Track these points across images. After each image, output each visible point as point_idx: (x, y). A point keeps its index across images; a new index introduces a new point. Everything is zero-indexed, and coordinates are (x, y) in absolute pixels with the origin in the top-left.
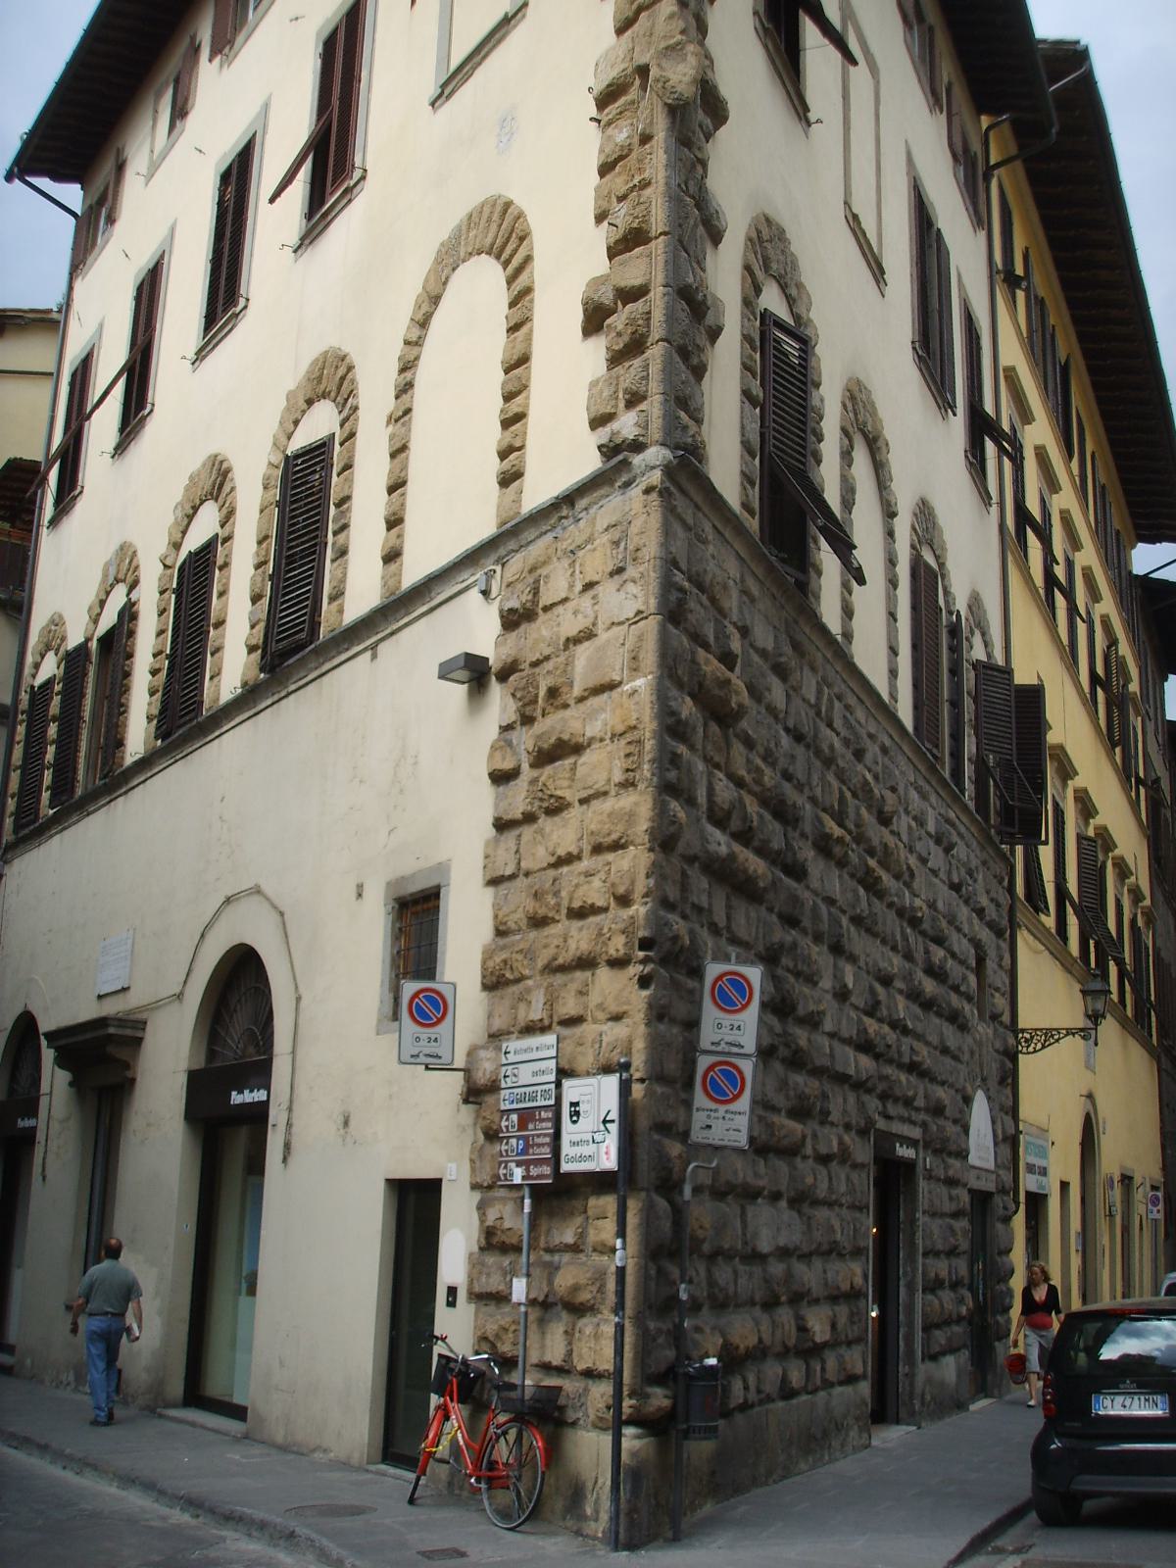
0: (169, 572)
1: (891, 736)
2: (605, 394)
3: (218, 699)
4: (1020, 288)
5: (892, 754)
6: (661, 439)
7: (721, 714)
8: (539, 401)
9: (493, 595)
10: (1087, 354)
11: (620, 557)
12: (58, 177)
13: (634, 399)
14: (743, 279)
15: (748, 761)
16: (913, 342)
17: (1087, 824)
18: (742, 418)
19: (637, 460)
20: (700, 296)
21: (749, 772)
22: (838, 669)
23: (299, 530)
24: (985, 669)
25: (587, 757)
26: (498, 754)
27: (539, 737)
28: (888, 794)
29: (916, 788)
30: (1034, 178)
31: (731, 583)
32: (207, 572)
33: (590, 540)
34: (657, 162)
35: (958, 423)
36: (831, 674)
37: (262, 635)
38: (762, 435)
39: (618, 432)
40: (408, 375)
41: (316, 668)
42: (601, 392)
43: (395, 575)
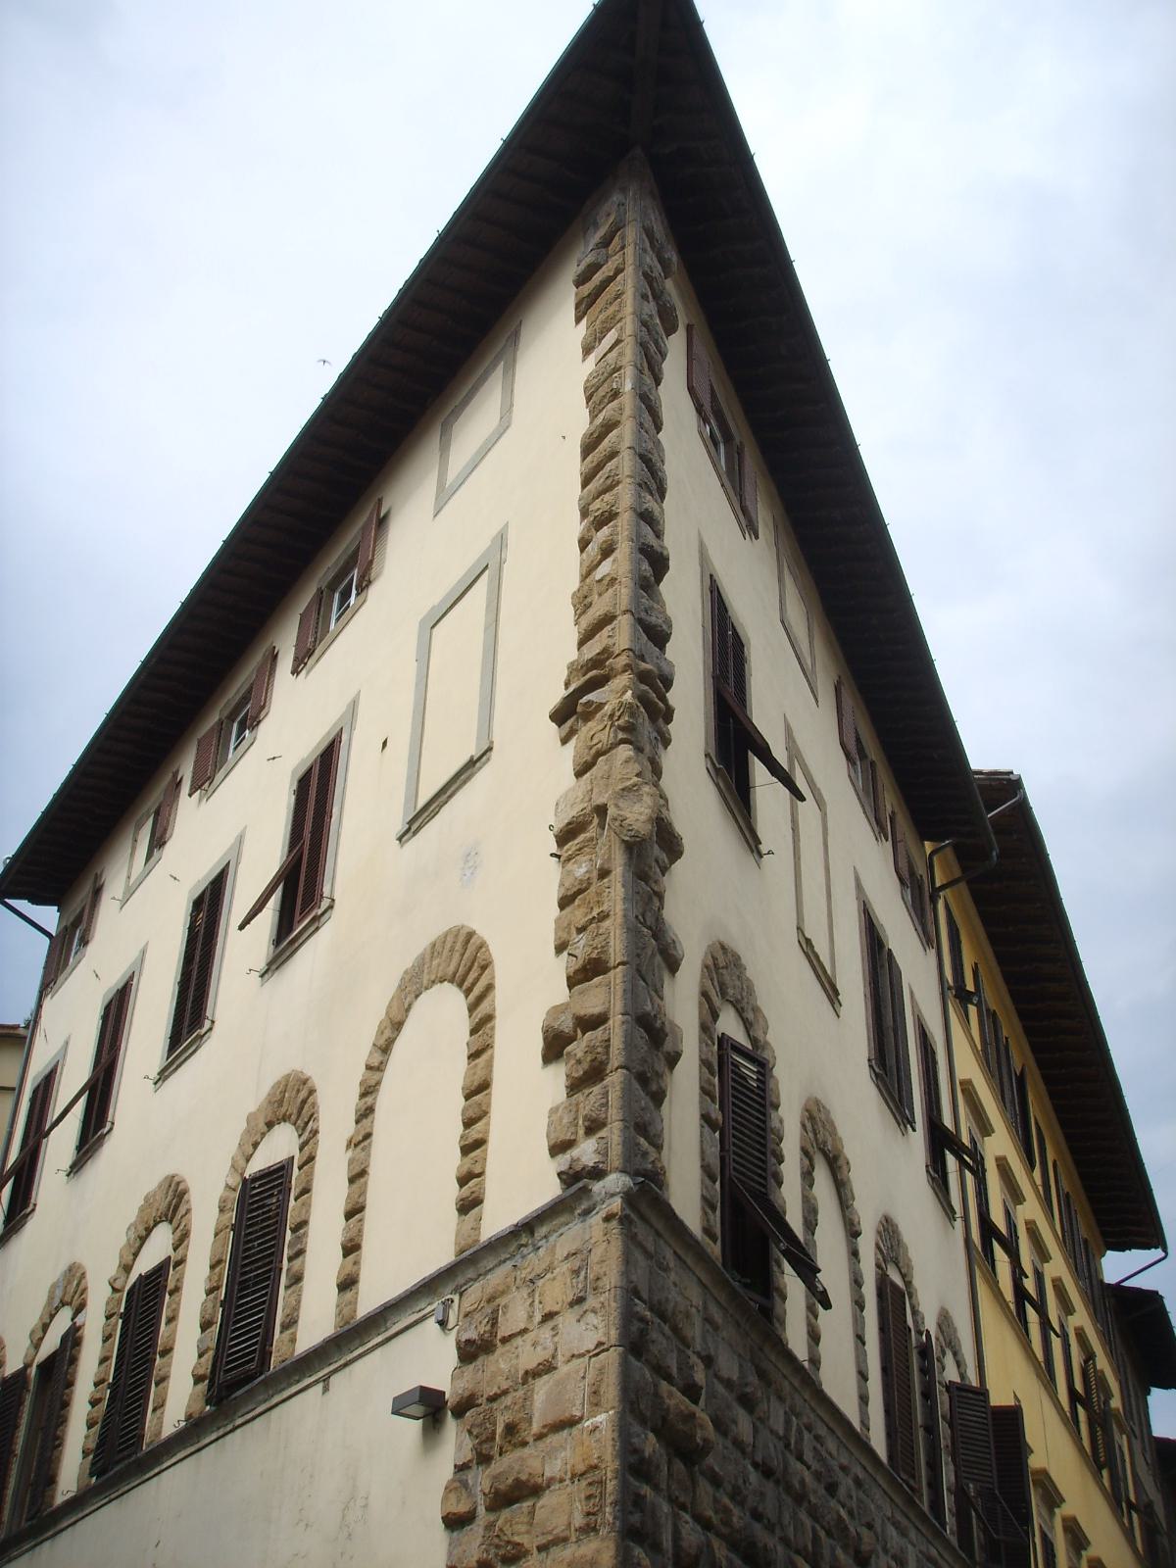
0: (118, 1295)
1: (865, 1468)
2: (565, 1121)
3: (160, 1433)
4: (972, 1003)
5: (867, 1487)
6: (620, 1167)
7: (686, 1450)
8: (499, 1128)
9: (450, 1326)
10: (1041, 1065)
11: (580, 1286)
12: (37, 900)
13: (593, 1127)
14: (700, 1004)
15: (716, 1501)
16: (869, 1060)
17: (1079, 1556)
18: (702, 1141)
19: (597, 1187)
20: (658, 1024)
21: (716, 1513)
22: (806, 1397)
23: (254, 1255)
24: (960, 1391)
25: (547, 1500)
26: (453, 1497)
27: (496, 1478)
28: (864, 1531)
29: (894, 1524)
30: (979, 899)
31: (694, 1310)
32: (156, 1297)
33: (550, 1269)
34: (615, 895)
35: (918, 1138)
36: (799, 1402)
37: (210, 1363)
38: (722, 1159)
39: (578, 1159)
40: (369, 1100)
41: (265, 1401)
42: (561, 1118)
43: (350, 1303)
